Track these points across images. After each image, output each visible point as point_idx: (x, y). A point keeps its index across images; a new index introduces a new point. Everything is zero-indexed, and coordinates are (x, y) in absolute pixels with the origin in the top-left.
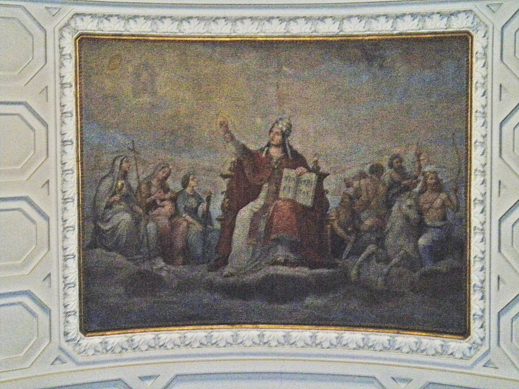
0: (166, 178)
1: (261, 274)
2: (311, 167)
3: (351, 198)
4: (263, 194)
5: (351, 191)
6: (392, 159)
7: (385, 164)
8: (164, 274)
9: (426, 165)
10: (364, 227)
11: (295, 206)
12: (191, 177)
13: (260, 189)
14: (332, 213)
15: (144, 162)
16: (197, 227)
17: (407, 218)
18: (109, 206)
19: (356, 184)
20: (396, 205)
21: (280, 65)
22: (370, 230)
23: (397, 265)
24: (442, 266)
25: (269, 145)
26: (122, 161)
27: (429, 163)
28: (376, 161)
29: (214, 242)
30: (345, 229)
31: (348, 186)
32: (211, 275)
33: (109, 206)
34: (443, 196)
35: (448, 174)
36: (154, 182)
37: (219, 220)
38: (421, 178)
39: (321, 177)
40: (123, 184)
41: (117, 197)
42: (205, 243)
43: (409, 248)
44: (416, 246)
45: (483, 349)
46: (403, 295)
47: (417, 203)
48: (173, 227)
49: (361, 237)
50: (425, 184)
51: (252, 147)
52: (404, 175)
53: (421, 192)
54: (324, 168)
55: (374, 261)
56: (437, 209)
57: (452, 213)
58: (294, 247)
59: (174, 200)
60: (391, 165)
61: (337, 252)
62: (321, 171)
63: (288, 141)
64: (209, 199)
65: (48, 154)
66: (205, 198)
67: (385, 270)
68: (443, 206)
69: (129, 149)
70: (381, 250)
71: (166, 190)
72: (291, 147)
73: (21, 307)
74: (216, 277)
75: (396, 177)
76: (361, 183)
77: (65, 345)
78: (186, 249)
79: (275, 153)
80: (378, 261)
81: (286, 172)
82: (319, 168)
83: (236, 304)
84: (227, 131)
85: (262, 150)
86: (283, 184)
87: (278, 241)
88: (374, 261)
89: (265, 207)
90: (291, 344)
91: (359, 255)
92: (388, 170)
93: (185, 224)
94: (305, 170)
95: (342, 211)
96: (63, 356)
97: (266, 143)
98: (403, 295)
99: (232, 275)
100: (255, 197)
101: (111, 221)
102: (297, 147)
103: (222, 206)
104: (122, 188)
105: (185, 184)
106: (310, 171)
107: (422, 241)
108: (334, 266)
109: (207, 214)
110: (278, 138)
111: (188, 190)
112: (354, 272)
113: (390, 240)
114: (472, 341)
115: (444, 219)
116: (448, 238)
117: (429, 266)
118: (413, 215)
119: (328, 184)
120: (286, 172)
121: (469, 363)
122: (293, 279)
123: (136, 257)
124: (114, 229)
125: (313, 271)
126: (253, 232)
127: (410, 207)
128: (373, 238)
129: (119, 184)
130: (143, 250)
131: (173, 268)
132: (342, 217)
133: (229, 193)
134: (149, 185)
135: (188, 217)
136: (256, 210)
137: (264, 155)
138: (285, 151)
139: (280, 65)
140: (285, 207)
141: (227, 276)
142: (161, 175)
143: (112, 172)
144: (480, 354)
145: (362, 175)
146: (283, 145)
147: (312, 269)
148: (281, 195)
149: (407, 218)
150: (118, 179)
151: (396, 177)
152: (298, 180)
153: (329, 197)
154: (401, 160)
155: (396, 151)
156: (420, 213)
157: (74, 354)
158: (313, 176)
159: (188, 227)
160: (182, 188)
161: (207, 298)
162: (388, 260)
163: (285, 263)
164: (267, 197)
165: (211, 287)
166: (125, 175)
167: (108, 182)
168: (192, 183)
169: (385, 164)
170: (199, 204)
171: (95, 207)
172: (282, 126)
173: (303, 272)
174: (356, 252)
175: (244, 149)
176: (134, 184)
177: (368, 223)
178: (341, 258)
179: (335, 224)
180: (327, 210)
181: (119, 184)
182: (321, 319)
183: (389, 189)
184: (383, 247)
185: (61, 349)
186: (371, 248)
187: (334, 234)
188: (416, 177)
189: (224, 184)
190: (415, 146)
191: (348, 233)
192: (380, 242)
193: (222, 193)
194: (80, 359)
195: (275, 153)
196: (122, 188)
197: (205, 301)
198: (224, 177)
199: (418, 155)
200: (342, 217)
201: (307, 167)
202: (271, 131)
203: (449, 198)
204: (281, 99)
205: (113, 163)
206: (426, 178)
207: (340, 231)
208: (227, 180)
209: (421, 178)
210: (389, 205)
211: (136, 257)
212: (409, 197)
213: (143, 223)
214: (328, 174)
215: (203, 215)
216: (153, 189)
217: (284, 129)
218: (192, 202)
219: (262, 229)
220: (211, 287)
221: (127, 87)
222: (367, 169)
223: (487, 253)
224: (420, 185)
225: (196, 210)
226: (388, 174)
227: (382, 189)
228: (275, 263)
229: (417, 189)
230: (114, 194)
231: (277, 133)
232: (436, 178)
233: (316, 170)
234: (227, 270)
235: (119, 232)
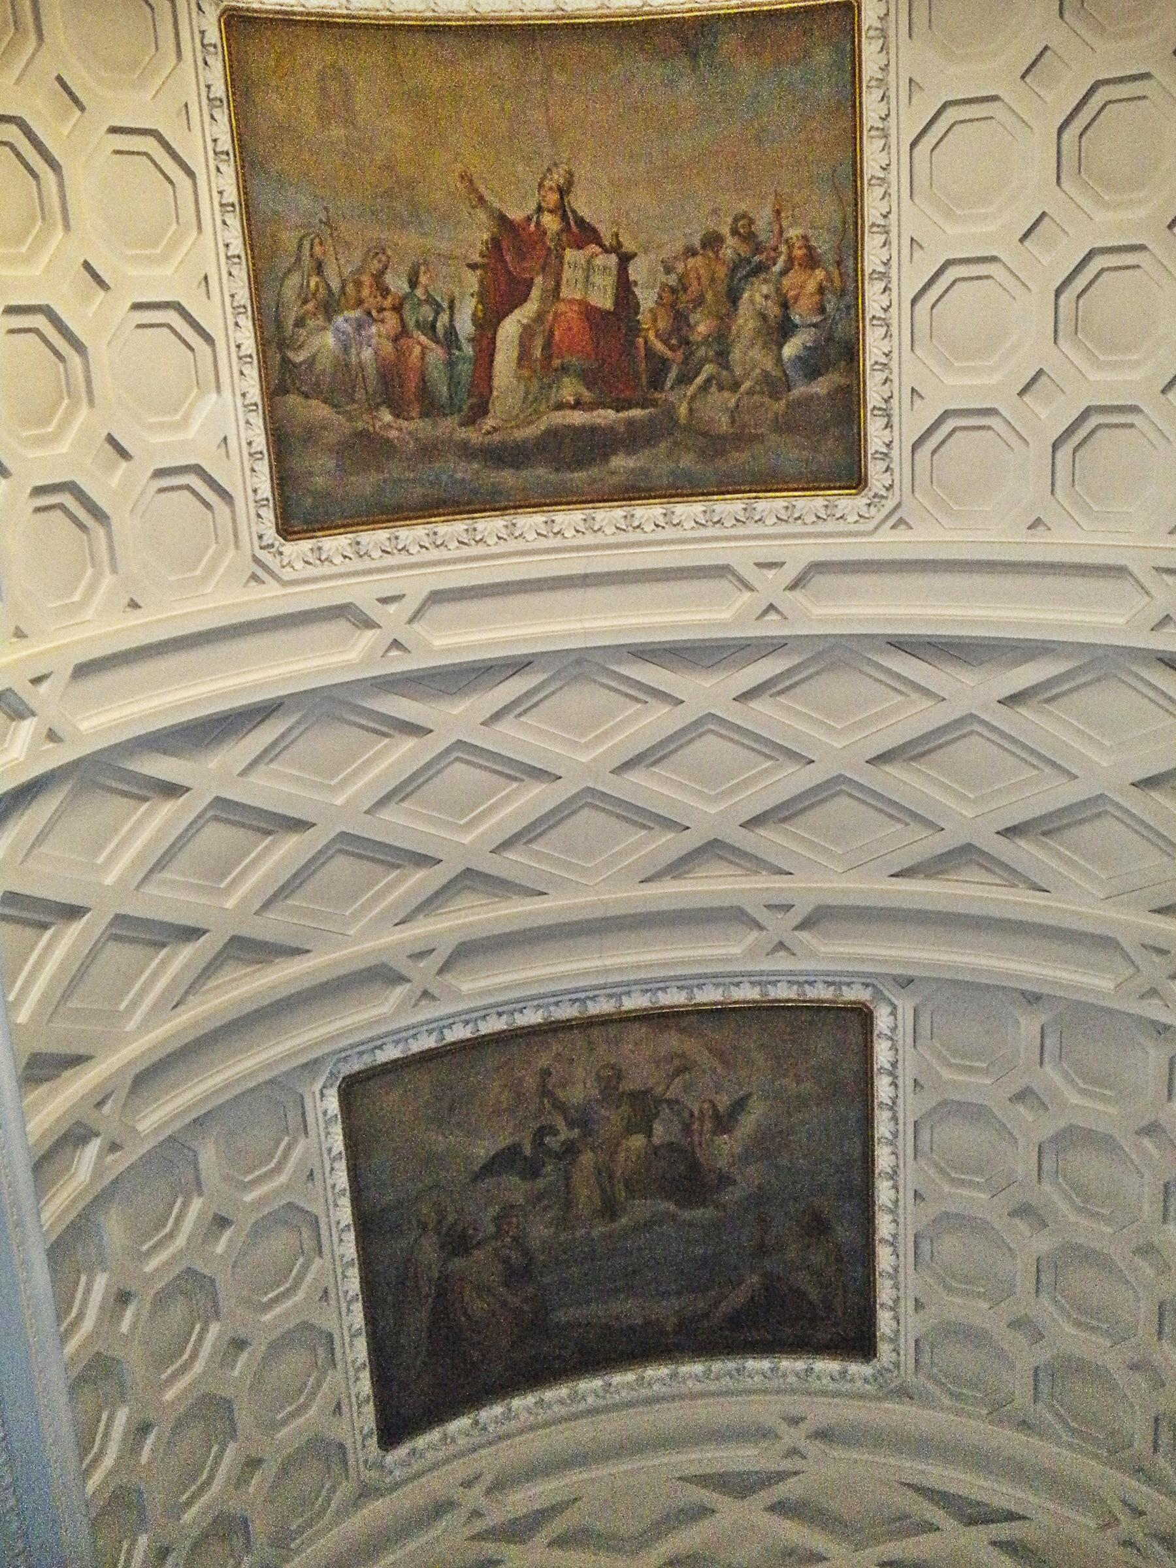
0: (382, 272)
1: (543, 425)
2: (607, 244)
3: (673, 291)
4: (535, 293)
5: (672, 280)
6: (736, 220)
7: (725, 230)
8: (393, 434)
9: (791, 226)
10: (695, 337)
11: (589, 313)
12: (423, 268)
13: (529, 284)
14: (644, 317)
15: (348, 245)
16: (437, 354)
17: (763, 317)
18: (300, 323)
19: (680, 267)
20: (746, 295)
21: (548, 69)
22: (705, 341)
23: (750, 392)
24: (820, 387)
25: (540, 209)
26: (312, 240)
27: (795, 223)
28: (711, 225)
29: (465, 379)
30: (665, 342)
31: (668, 270)
32: (463, 434)
33: (300, 323)
34: (820, 274)
35: (826, 236)
36: (366, 279)
37: (471, 340)
38: (783, 248)
39: (625, 259)
40: (317, 285)
41: (310, 306)
42: (453, 382)
43: (768, 364)
44: (779, 360)
45: (890, 504)
46: (760, 438)
47: (778, 290)
48: (401, 354)
49: (692, 353)
50: (791, 259)
51: (516, 214)
52: (758, 249)
53: (784, 273)
54: (629, 245)
55: (714, 389)
56: (812, 294)
57: (834, 300)
58: (588, 378)
59: (397, 309)
60: (735, 232)
61: (656, 383)
62: (623, 250)
63: (569, 202)
64: (451, 307)
65: (171, 182)
66: (445, 305)
67: (732, 403)
68: (821, 290)
69: (321, 221)
70: (724, 373)
71: (385, 292)
72: (574, 212)
73: (186, 493)
74: (472, 436)
75: (744, 250)
76: (689, 267)
77: (264, 555)
78: (425, 391)
79: (551, 222)
80: (721, 388)
81: (570, 254)
82: (620, 245)
83: (507, 477)
84: (472, 188)
85: (529, 219)
86: (567, 274)
87: (564, 369)
88: (714, 389)
89: (539, 317)
90: (595, 531)
91: (691, 381)
92: (731, 241)
93: (417, 350)
94: (598, 249)
95: (661, 312)
96: (260, 572)
97: (534, 206)
98: (760, 438)
99: (495, 429)
100: (525, 298)
101: (306, 347)
102: (585, 212)
103: (474, 314)
104: (317, 290)
105: (413, 284)
106: (606, 251)
107: (790, 350)
108: (653, 403)
109: (451, 330)
110: (553, 198)
111: (419, 292)
112: (683, 410)
113: (736, 354)
114: (871, 494)
115: (822, 310)
116: (830, 339)
117: (800, 390)
118: (773, 310)
119: (638, 271)
120: (570, 254)
121: (871, 525)
122: (593, 429)
123: (348, 408)
124: (311, 361)
125: (621, 415)
126: (524, 357)
127: (767, 297)
128: (711, 353)
129: (312, 284)
130: (360, 395)
131: (405, 424)
132: (661, 325)
133: (482, 296)
134: (358, 284)
135: (423, 338)
136: (525, 321)
137: (532, 227)
138: (564, 217)
139: (548, 69)
140: (571, 314)
141: (489, 433)
142: (375, 266)
143: (299, 260)
144: (885, 511)
145: (691, 252)
146: (562, 210)
147: (618, 411)
148: (565, 293)
149: (763, 317)
150: (309, 275)
151: (744, 250)
152: (589, 265)
153: (637, 291)
154: (751, 222)
155: (743, 207)
156: (785, 305)
157: (277, 570)
158: (613, 259)
159: (423, 353)
160: (408, 290)
161: (464, 470)
162: (735, 386)
163: (577, 405)
164: (543, 300)
165: (467, 451)
166: (319, 268)
167: (294, 280)
168: (423, 279)
169: (725, 230)
170: (437, 313)
171: (279, 324)
172: (558, 177)
173: (606, 416)
174: (684, 379)
175: (502, 220)
176: (335, 285)
177: (702, 329)
178: (662, 389)
179: (651, 335)
180: (637, 313)
181: (312, 284)
182: (639, 490)
183: (734, 270)
184: (726, 366)
185: (256, 560)
186: (708, 369)
187: (650, 353)
188: (775, 249)
189: (472, 280)
190: (772, 197)
191: (672, 348)
192: (722, 357)
193: (472, 295)
194: (287, 574)
195: (551, 222)
196: (317, 290)
197: (459, 475)
198: (473, 267)
199: (778, 212)
200: (661, 325)
201: (601, 245)
202: (541, 185)
203: (828, 273)
204: (555, 135)
205: (300, 246)
206: (790, 247)
207: (659, 346)
208: (478, 272)
209: (783, 248)
210: (734, 297)
211: (348, 408)
212: (765, 281)
213: (353, 351)
214: (635, 255)
215: (446, 333)
216: (366, 292)
217: (562, 181)
218: (427, 312)
219: (538, 353)
220: (467, 451)
221: (309, 113)
222: (697, 243)
223: (895, 355)
224: (782, 258)
225: (433, 327)
226: (731, 248)
227: (722, 272)
228: (560, 406)
229: (777, 269)
230: (305, 302)
231: (551, 188)
232: (810, 248)
233: (616, 248)
234: (489, 423)
235: (319, 367)
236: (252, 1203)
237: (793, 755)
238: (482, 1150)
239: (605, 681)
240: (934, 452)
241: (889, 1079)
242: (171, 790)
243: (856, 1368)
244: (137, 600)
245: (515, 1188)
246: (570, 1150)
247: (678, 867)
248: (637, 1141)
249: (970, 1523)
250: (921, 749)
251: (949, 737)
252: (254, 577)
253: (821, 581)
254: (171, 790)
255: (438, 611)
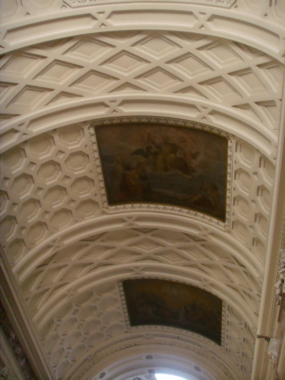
96: (65, 5)
236: (62, 158)
237: (211, 68)
238: (133, 148)
239: (163, 38)
240: (56, 63)
241: (230, 159)
242: (44, 57)
243: (221, 223)
244: (29, 12)
245: (141, 159)
246: (156, 154)
247: (184, 90)
248: (172, 155)
249: (2, 367)
250: (241, 73)
251: (244, 73)
252: (64, 6)
253: (216, 20)
254: (44, 57)
255: (115, 16)
